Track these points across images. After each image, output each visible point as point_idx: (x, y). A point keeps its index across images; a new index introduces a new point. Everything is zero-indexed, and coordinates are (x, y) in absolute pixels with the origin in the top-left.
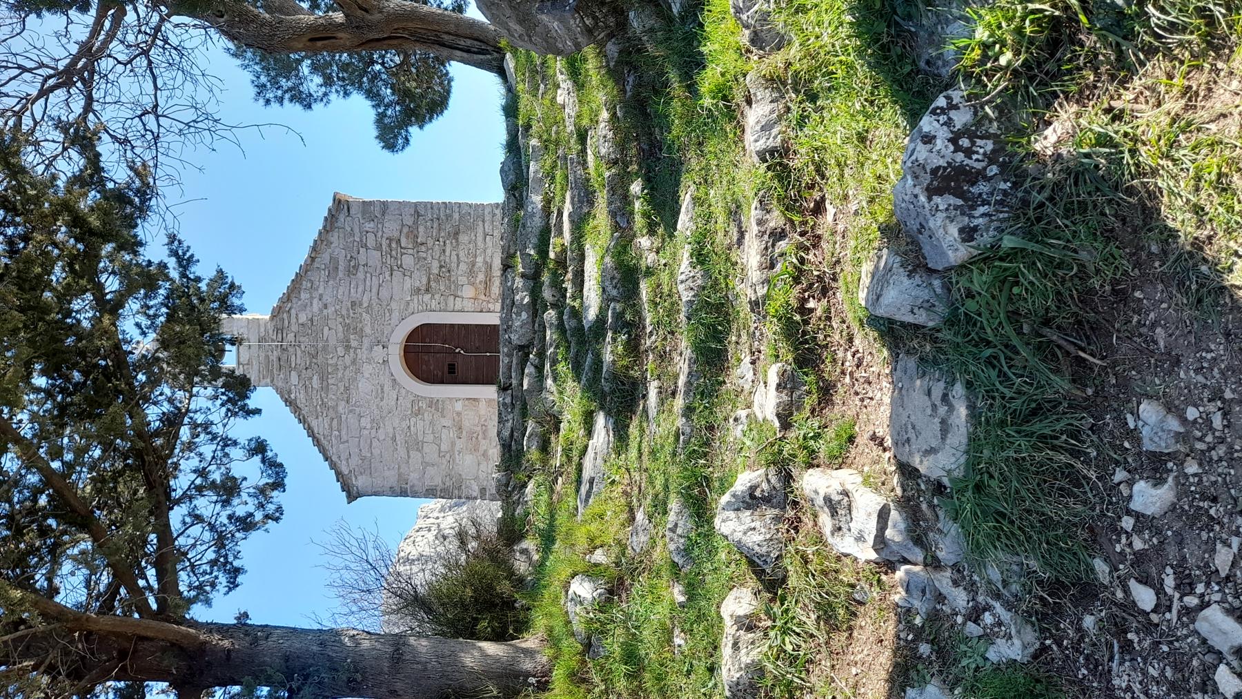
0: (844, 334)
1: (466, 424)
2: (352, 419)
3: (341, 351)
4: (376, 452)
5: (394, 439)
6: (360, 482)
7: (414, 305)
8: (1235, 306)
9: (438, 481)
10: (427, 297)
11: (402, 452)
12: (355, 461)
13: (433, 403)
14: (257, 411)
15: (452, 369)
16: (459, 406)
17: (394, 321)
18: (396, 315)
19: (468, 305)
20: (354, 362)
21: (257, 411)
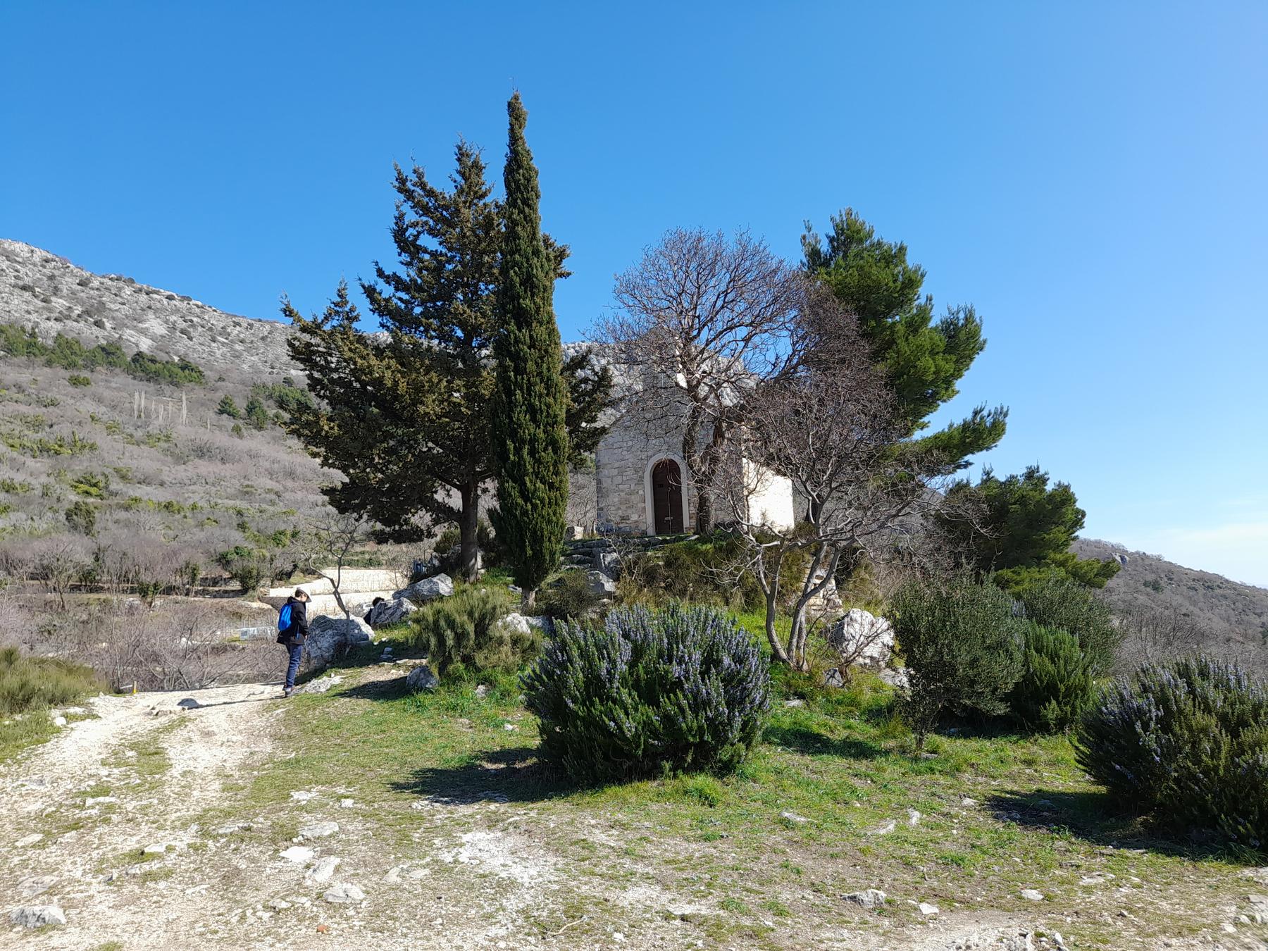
11: (617, 465)
13: (642, 478)
14: (569, 274)
15: (661, 486)
16: (641, 492)
21: (569, 274)
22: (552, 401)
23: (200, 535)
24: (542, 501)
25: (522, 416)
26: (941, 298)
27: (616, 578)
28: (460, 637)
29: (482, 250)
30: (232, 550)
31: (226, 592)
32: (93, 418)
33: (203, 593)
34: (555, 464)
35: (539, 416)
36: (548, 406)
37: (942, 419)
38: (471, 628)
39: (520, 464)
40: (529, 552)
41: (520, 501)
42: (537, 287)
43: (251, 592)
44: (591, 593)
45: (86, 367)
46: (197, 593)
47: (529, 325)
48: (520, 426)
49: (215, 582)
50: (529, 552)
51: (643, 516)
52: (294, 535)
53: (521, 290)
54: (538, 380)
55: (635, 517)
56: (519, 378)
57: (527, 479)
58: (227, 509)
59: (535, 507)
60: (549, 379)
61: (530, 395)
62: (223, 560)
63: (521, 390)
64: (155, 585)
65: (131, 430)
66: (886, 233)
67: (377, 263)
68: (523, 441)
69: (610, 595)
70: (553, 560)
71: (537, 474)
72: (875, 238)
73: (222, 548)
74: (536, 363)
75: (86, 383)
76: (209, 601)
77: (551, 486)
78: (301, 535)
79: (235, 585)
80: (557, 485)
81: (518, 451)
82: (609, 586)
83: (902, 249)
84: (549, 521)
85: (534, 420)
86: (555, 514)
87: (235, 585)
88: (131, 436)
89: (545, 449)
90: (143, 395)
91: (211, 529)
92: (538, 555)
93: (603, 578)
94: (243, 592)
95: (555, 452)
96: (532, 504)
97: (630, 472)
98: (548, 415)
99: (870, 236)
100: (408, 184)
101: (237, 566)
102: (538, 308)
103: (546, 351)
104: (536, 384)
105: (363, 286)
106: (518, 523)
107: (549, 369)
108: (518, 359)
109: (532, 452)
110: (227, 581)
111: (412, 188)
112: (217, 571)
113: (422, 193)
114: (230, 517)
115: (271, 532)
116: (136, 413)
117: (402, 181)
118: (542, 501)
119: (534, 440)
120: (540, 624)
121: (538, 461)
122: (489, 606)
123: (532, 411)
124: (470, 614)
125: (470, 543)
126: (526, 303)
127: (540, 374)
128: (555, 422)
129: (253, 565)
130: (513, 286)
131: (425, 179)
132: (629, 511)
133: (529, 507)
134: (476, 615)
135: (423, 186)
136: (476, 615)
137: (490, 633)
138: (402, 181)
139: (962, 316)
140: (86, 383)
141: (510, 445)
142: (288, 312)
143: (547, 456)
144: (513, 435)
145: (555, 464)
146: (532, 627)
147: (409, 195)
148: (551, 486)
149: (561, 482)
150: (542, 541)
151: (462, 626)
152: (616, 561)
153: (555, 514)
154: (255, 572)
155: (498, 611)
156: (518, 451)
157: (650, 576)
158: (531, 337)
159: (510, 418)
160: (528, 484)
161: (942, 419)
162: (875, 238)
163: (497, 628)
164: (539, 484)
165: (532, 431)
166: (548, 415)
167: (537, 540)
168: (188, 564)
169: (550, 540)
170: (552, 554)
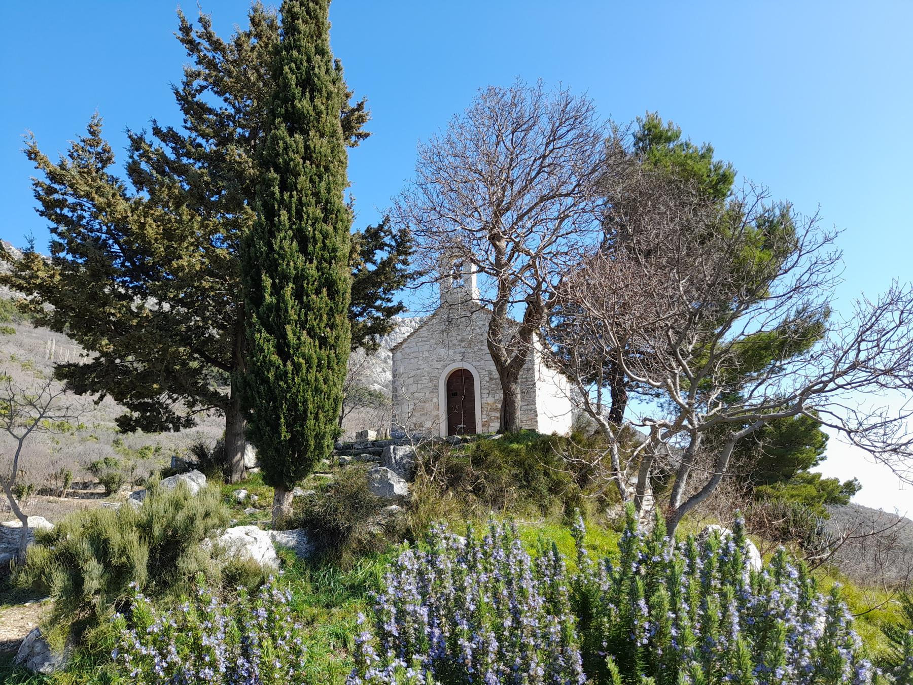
0: (331, 383)
1: (427, 405)
2: (427, 347)
3: (459, 338)
4: (412, 361)
5: (419, 369)
6: (399, 354)
7: (483, 373)
8: (879, 537)
9: (400, 393)
10: (487, 379)
11: (412, 374)
12: (408, 350)
13: (436, 388)
14: (367, 135)
15: (455, 394)
16: (435, 400)
17: (474, 364)
18: (478, 364)
19: (484, 401)
20: (454, 345)
21: (367, 135)
22: (330, 229)
23: (80, 448)
24: (308, 360)
25: (286, 244)
26: (756, 188)
27: (410, 475)
28: (118, 575)
29: (272, 109)
30: (102, 460)
31: (92, 494)
32: (12, 358)
33: (74, 494)
34: (331, 313)
35: (310, 248)
36: (325, 236)
37: (752, 323)
38: (140, 556)
39: (279, 309)
40: (285, 435)
41: (275, 358)
42: (320, 91)
43: (113, 495)
44: (374, 497)
45: (14, 321)
46: (68, 495)
47: (305, 133)
48: (283, 257)
49: (85, 486)
50: (285, 435)
51: (435, 419)
52: (157, 450)
53: (297, 91)
54: (313, 201)
55: (428, 424)
56: (286, 195)
57: (288, 327)
58: (108, 429)
59: (297, 367)
60: (328, 202)
61: (300, 218)
62: (93, 468)
63: (289, 212)
64: (30, 487)
65: (41, 368)
66: (694, 133)
67: (155, 122)
68: (285, 278)
69: (400, 500)
70: (319, 447)
71: (303, 324)
72: (683, 139)
73: (94, 458)
74: (311, 181)
75: (12, 332)
76: (76, 501)
77: (323, 342)
78: (162, 451)
79: (102, 489)
80: (331, 340)
81: (277, 290)
82: (400, 487)
83: (709, 150)
84: (317, 391)
85: (303, 250)
86: (326, 381)
87: (102, 489)
88: (41, 372)
89: (318, 292)
90: (54, 342)
91: (92, 444)
92: (298, 441)
93: (392, 477)
94: (107, 494)
95: (332, 295)
96: (293, 363)
97: (425, 380)
98: (325, 247)
99: (678, 137)
100: (193, 35)
101: (105, 471)
102: (319, 114)
103: (327, 169)
104: (308, 204)
105: (130, 137)
106: (270, 390)
107: (329, 191)
108: (287, 173)
109: (299, 294)
110: (96, 485)
111: (198, 40)
112: (89, 478)
113: (207, 45)
114: (109, 436)
115: (139, 447)
116: (48, 355)
117: (186, 30)
118: (308, 360)
119: (300, 278)
120: (292, 543)
121: (308, 307)
122: (181, 516)
123: (302, 239)
124: (145, 528)
125: (237, 435)
126: (304, 104)
127: (316, 194)
128: (335, 258)
129: (117, 473)
130: (287, 86)
131: (211, 29)
132: (423, 418)
133: (290, 367)
134: (157, 531)
135: (209, 37)
136: (157, 531)
137: (181, 563)
138: (186, 30)
139: (777, 212)
140: (12, 332)
141: (267, 281)
142: (32, 154)
143: (321, 301)
144: (273, 269)
145: (331, 313)
146: (278, 548)
147: (193, 46)
148: (323, 342)
149: (337, 338)
150: (304, 418)
151: (123, 551)
152: (412, 456)
153: (326, 381)
154: (117, 479)
155: (199, 525)
156: (277, 290)
157: (454, 477)
158: (307, 147)
159: (270, 246)
160: (290, 335)
161: (752, 323)
162: (683, 139)
163: (199, 557)
164: (304, 336)
165: (300, 264)
166: (325, 247)
167: (298, 417)
168: (62, 471)
169: (316, 418)
170: (319, 437)
